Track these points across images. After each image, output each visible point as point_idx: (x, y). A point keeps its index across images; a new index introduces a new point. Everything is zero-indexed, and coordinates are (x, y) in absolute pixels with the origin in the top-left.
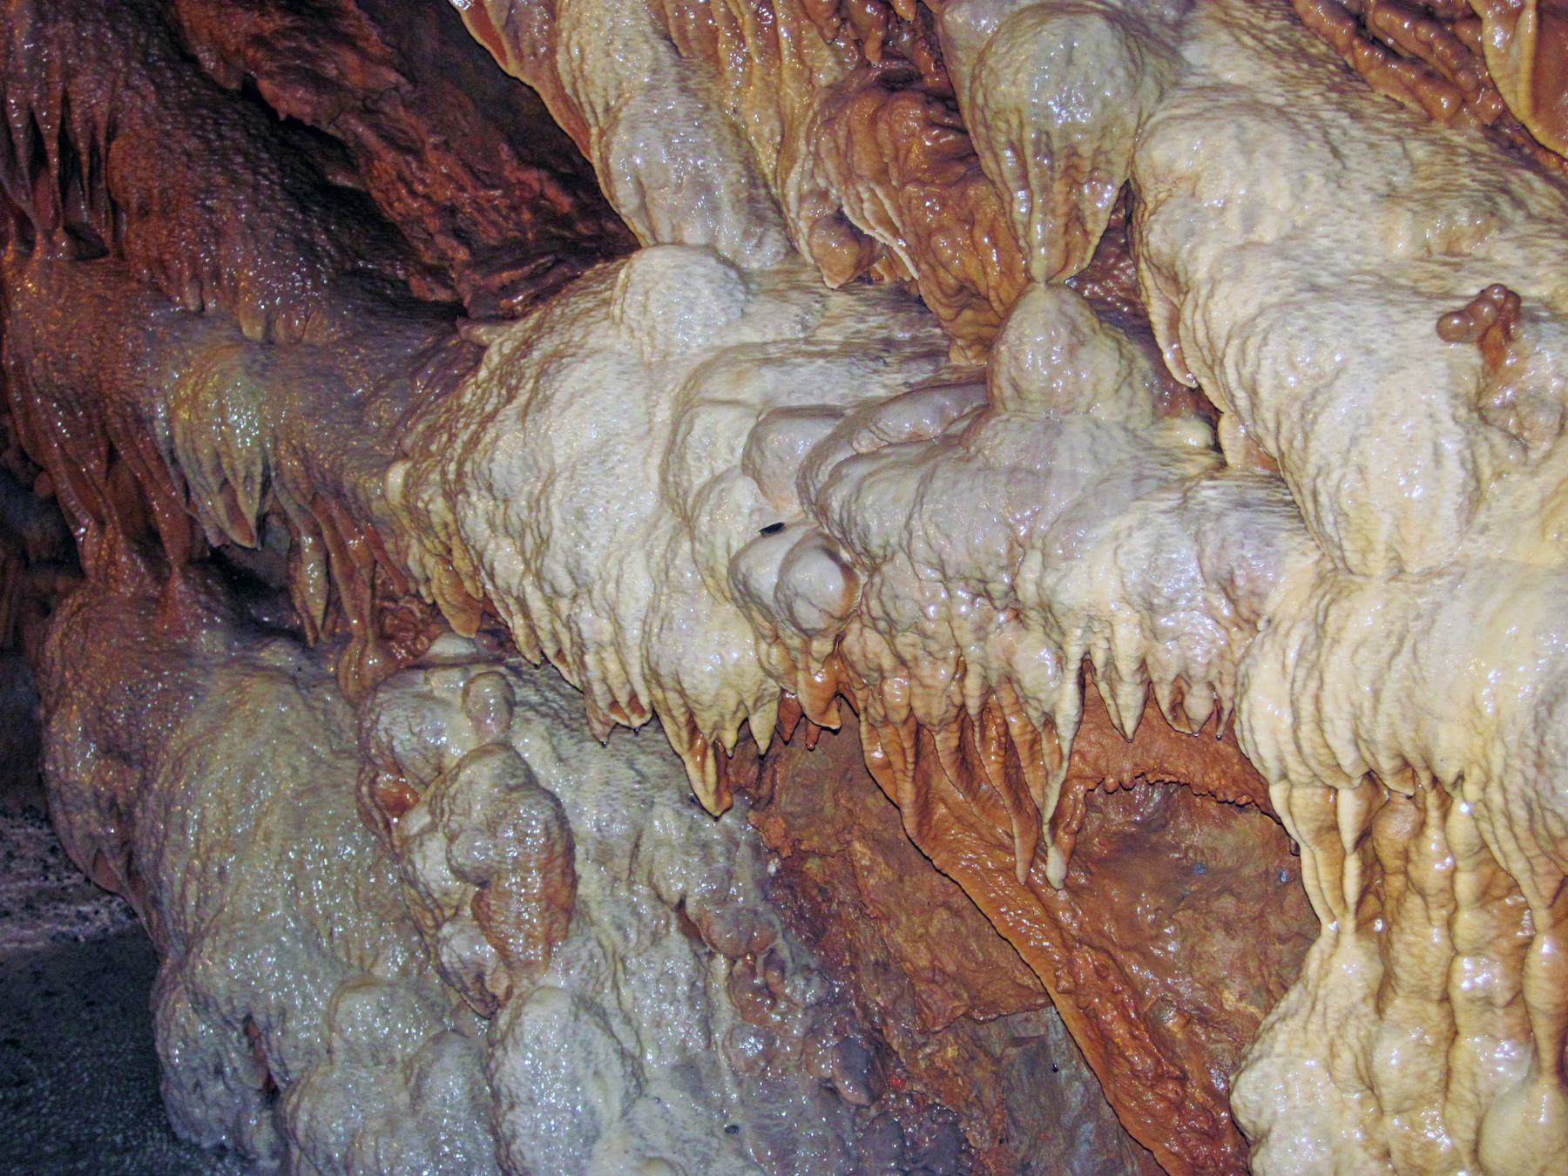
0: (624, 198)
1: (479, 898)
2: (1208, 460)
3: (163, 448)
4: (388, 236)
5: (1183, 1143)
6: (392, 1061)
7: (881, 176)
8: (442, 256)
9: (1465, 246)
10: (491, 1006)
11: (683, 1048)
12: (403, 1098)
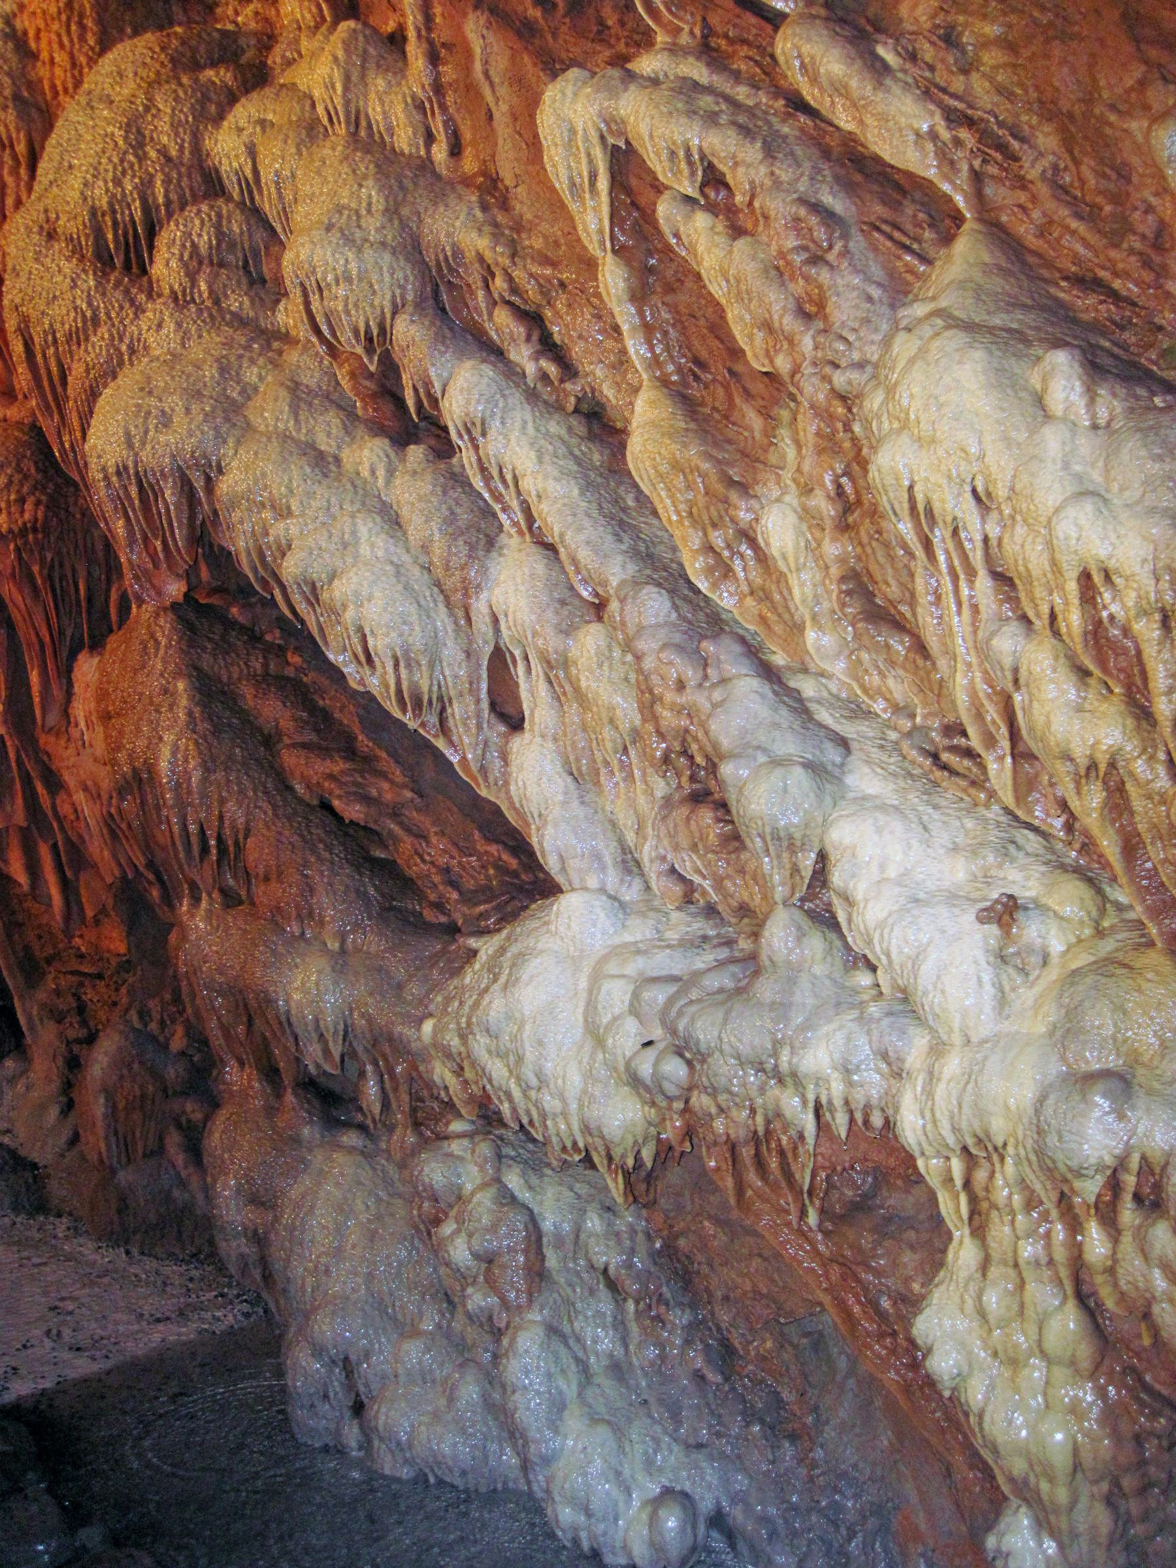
0: (552, 864)
1: (488, 1270)
2: (874, 992)
3: (283, 1018)
4: (407, 885)
5: (897, 1373)
6: (434, 1381)
7: (694, 847)
8: (441, 896)
9: (993, 872)
10: (497, 1334)
11: (611, 1356)
12: (443, 1402)
